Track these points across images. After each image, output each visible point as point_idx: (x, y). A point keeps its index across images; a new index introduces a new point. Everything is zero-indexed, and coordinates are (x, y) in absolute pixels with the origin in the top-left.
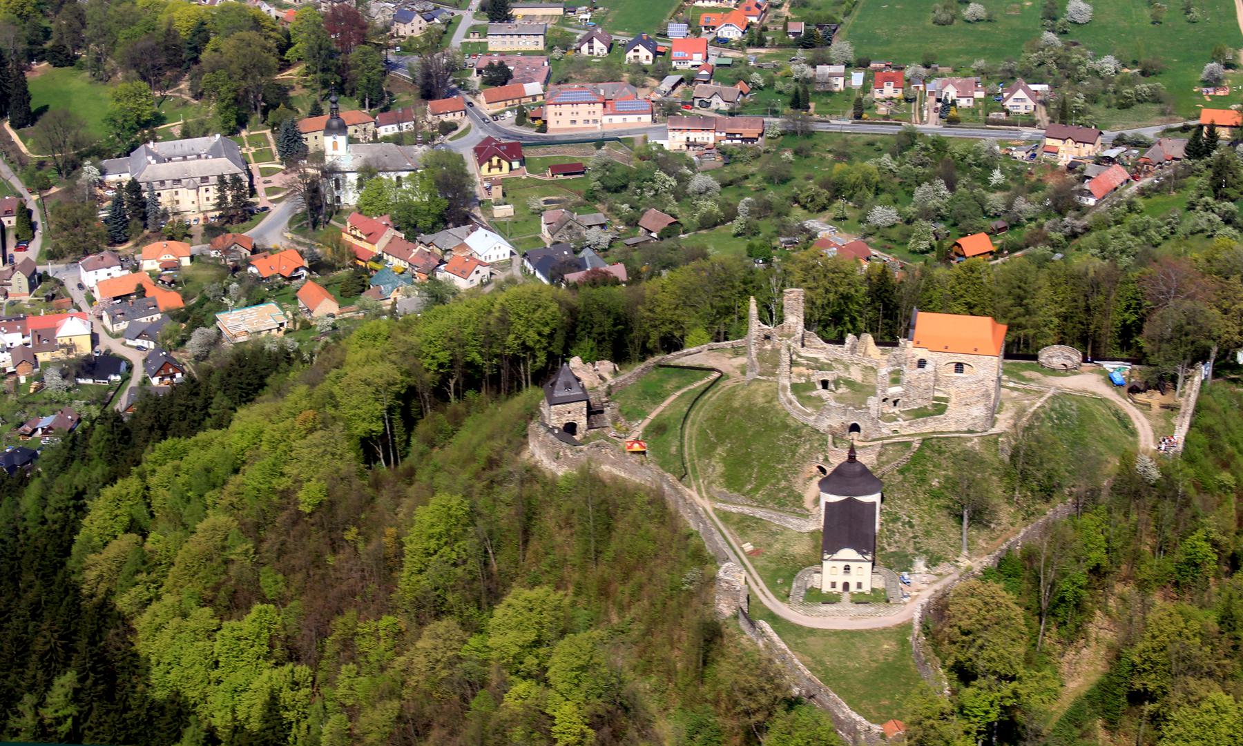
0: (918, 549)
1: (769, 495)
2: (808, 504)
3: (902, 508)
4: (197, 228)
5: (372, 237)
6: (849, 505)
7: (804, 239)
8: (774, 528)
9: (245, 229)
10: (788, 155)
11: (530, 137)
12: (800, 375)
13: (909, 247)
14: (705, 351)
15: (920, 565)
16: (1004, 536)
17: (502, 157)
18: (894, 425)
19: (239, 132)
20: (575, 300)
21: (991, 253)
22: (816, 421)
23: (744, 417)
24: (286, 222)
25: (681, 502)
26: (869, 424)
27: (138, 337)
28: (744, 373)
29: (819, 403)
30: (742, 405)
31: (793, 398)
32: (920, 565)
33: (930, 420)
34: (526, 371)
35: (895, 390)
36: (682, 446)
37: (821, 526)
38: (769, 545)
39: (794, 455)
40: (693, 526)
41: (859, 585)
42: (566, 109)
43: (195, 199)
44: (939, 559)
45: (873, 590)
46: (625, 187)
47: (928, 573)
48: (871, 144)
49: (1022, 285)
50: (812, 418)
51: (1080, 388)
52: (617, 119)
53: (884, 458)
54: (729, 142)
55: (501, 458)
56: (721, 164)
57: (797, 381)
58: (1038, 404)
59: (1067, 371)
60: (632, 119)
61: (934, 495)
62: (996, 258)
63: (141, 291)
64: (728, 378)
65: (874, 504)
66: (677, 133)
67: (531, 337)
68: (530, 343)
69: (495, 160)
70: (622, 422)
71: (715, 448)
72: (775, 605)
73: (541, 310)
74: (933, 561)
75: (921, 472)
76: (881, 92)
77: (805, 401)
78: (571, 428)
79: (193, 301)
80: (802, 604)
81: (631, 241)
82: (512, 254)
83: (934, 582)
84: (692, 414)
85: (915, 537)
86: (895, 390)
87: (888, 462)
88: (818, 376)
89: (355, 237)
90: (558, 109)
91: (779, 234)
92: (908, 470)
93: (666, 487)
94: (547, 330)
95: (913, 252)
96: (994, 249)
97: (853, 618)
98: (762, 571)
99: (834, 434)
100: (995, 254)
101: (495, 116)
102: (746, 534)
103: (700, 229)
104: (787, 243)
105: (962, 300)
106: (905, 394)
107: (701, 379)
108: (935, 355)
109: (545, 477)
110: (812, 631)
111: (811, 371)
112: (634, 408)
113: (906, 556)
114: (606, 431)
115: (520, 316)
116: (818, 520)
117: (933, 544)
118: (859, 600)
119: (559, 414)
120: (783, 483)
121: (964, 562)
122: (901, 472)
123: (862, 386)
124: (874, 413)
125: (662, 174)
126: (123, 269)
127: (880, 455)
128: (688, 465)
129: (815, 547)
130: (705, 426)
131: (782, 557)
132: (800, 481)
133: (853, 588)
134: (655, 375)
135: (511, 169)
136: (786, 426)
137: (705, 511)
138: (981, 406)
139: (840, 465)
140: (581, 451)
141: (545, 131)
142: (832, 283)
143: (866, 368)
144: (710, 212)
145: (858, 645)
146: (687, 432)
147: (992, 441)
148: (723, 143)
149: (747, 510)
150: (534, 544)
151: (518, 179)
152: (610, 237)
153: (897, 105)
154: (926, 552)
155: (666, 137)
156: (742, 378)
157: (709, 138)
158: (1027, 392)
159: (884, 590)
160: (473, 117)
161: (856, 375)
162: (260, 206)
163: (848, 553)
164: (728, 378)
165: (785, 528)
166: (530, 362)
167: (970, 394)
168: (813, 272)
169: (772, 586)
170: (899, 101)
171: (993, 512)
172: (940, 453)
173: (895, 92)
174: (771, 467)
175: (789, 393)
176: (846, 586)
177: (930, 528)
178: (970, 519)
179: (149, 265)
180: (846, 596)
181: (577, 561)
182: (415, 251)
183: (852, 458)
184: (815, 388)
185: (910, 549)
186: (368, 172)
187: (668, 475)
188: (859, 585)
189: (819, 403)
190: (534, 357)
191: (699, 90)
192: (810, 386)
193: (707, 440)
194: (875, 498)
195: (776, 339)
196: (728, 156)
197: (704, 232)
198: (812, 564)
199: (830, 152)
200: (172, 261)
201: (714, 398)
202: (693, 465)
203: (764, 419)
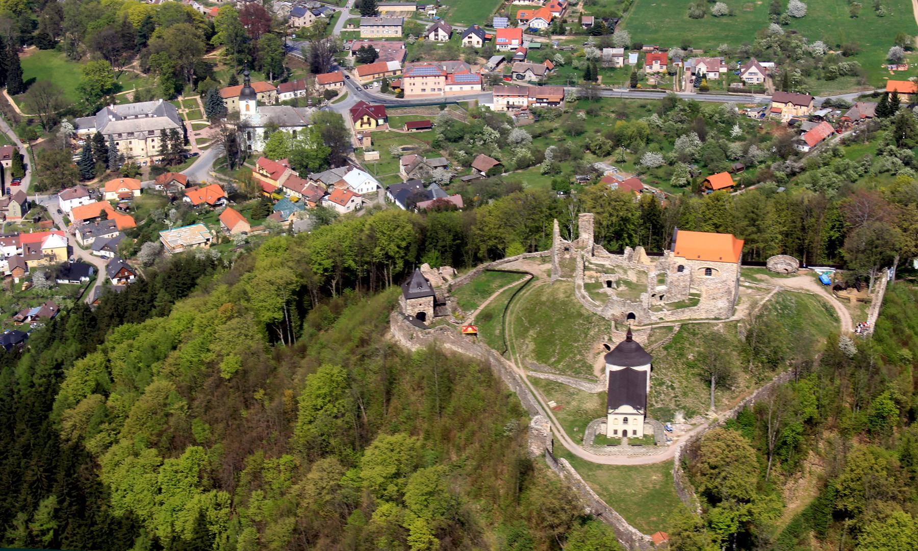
0: (678, 406)
1: (568, 366)
2: (597, 372)
3: (666, 375)
4: (146, 168)
5: (274, 175)
6: (627, 373)
7: (594, 176)
8: (572, 390)
9: (181, 169)
10: (582, 114)
11: (391, 101)
12: (591, 277)
13: (671, 182)
14: (521, 260)
15: (679, 417)
16: (742, 396)
17: (370, 116)
18: (660, 314)
19: (176, 97)
20: (425, 221)
21: (732, 187)
22: (602, 311)
23: (549, 308)
24: (211, 164)
25: (503, 371)
26: (642, 313)
27: (102, 249)
28: (549, 276)
29: (605, 298)
30: (548, 299)
31: (586, 294)
32: (679, 417)
33: (686, 310)
34: (388, 274)
35: (661, 288)
36: (504, 329)
37: (606, 389)
38: (568, 403)
39: (586, 336)
40: (512, 388)
41: (635, 432)
42: (418, 80)
43: (144, 147)
44: (693, 413)
45: (645, 436)
46: (461, 138)
47: (685, 423)
48: (643, 106)
49: (755, 210)
50: (600, 309)
51: (798, 287)
52: (456, 88)
53: (653, 339)
54: (538, 105)
55: (370, 338)
56: (532, 121)
57: (589, 281)
58: (767, 299)
59: (788, 274)
60: (467, 88)
61: (690, 365)
62: (735, 191)
63: (104, 215)
64: (538, 279)
65: (645, 372)
66: (500, 98)
67: (392, 249)
68: (391, 254)
69: (365, 118)
70: (460, 312)
71: (528, 331)
72: (572, 447)
73: (399, 229)
74: (689, 414)
75: (680, 349)
76: (651, 68)
77: (595, 296)
78: (421, 316)
79: (143, 223)
80: (592, 446)
81: (466, 178)
82: (378, 187)
83: (690, 430)
84: (511, 306)
85: (676, 397)
86: (661, 288)
87: (656, 341)
88: (604, 278)
89: (262, 175)
90: (412, 80)
91: (576, 173)
92: (671, 347)
93: (492, 360)
94: (404, 244)
95: (674, 186)
96: (734, 184)
97: (630, 457)
98: (562, 422)
99: (616, 321)
100: (735, 188)
101: (366, 86)
102: (551, 395)
103: (517, 169)
104: (581, 179)
105: (710, 222)
106: (669, 291)
107: (518, 280)
108: (690, 263)
109: (403, 352)
110: (599, 466)
111: (599, 274)
112: (469, 301)
113: (669, 411)
114: (447, 318)
115: (384, 234)
116: (604, 384)
117: (689, 402)
118: (635, 443)
119: (413, 306)
120: (578, 357)
121: (712, 415)
122: (666, 348)
123: (637, 285)
124: (645, 305)
125: (489, 128)
126: (91, 198)
127: (650, 336)
128: (508, 343)
129: (602, 404)
130: (520, 315)
131: (578, 412)
132: (591, 355)
133: (630, 434)
134: (483, 277)
135: (377, 125)
136: (580, 315)
137: (521, 377)
138: (724, 300)
139: (621, 344)
140: (429, 333)
141: (402, 97)
142: (614, 209)
143: (640, 272)
144: (524, 157)
145: (634, 476)
146: (507, 319)
147: (733, 326)
148: (534, 105)
149: (551, 377)
150: (394, 402)
151: (382, 132)
152: (450, 175)
153: (663, 77)
154: (684, 408)
155: (492, 102)
156: (548, 279)
157: (523, 102)
158: (759, 289)
159: (653, 436)
160: (349, 87)
161: (632, 277)
162: (192, 152)
163: (626, 409)
164: (538, 279)
165: (580, 390)
166: (391, 268)
167: (716, 291)
168: (601, 201)
169: (570, 433)
170: (664, 74)
171: (734, 378)
172: (694, 334)
173: (661, 68)
174: (569, 345)
175: (583, 291)
176: (625, 433)
177: (687, 390)
178: (716, 383)
179: (110, 196)
180: (625, 440)
181: (426, 414)
182: (307, 185)
183: (629, 339)
184: (602, 287)
185: (672, 406)
186: (271, 127)
187: (493, 351)
188: (635, 432)
189: (605, 298)
190: (395, 264)
191: (516, 66)
192: (598, 285)
193: (522, 325)
194: (647, 368)
195: (573, 250)
196: (538, 115)
197: (520, 171)
198: (599, 417)
199: (613, 112)
200: (127, 193)
201: (528, 294)
202: (512, 343)
203: (564, 310)
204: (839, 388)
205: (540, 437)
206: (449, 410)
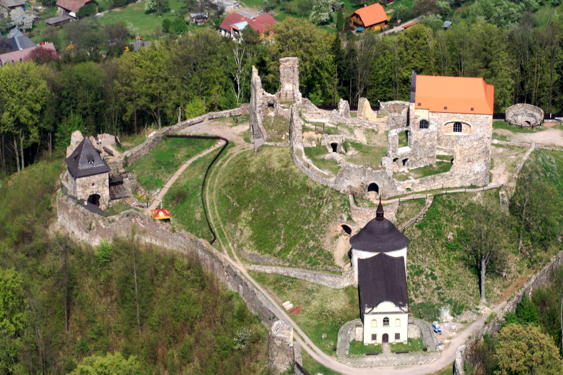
0: (442, 300)
1: (300, 255)
2: (339, 261)
3: (423, 261)
6: (381, 259)
7: (213, 13)
8: (309, 287)
12: (310, 140)
14: (206, 121)
15: (446, 314)
16: (514, 284)
18: (407, 184)
20: (59, 78)
21: (386, 22)
22: (336, 182)
25: (217, 265)
26: (386, 183)
28: (247, 140)
29: (333, 166)
30: (258, 171)
31: (309, 161)
32: (446, 314)
33: (437, 177)
34: (19, 148)
35: (404, 150)
36: (205, 212)
38: (308, 303)
39: (318, 216)
40: (231, 287)
41: (397, 336)
44: (462, 308)
45: (409, 340)
47: (454, 321)
49: (488, 48)
50: (332, 180)
51: (548, 143)
53: (402, 215)
55: (33, 231)
57: (308, 145)
59: (532, 128)
61: (450, 247)
62: (391, 27)
64: (233, 145)
65: (402, 258)
67: (24, 113)
68: (23, 120)
70: (142, 192)
71: (239, 213)
72: (324, 359)
73: (32, 87)
74: (457, 310)
75: (436, 227)
77: (322, 163)
78: (94, 199)
80: (348, 356)
81: (52, 21)
83: (462, 330)
84: (209, 181)
85: (438, 288)
86: (404, 150)
87: (407, 218)
88: (327, 140)
91: (190, 10)
92: (426, 225)
93: (200, 253)
94: (38, 107)
96: (388, 19)
98: (305, 327)
99: (354, 195)
100: (391, 23)
102: (284, 293)
104: (198, 18)
105: (409, 66)
106: (413, 154)
107: (209, 147)
108: (435, 116)
109: (80, 248)
111: (319, 136)
112: (152, 177)
113: (433, 307)
114: (128, 201)
115: (12, 94)
116: (352, 278)
117: (455, 294)
119: (84, 187)
120: (312, 243)
121: (486, 311)
122: (420, 227)
123: (369, 148)
124: (390, 173)
127: (399, 212)
128: (215, 230)
129: (351, 302)
130: (224, 192)
131: (321, 313)
132: (328, 240)
133: (392, 339)
134: (165, 146)
136: (307, 189)
137: (241, 273)
138: (481, 161)
139: (369, 223)
140: (113, 221)
142: (307, 51)
143: (368, 130)
146: (207, 198)
147: (495, 193)
149: (281, 271)
150: (76, 314)
152: (33, 17)
154: (450, 302)
156: (246, 145)
158: (511, 148)
159: (421, 340)
161: (360, 137)
163: (387, 306)
164: (233, 145)
165: (320, 286)
166: (22, 139)
167: (472, 151)
168: (290, 42)
169: (318, 341)
171: (503, 262)
172: (451, 208)
174: (297, 229)
175: (304, 157)
176: (385, 337)
177: (450, 279)
178: (487, 269)
180: (386, 346)
181: (120, 327)
183: (380, 216)
184: (326, 151)
185: (435, 300)
187: (201, 240)
188: (397, 336)
189: (333, 166)
190: (27, 134)
192: (321, 149)
193: (228, 203)
194: (402, 253)
195: (279, 106)
197: (117, 10)
198: (350, 318)
201: (225, 165)
202: (219, 229)
203: (283, 183)
204: (83, 345)
205: (284, 347)
206: (154, 319)
